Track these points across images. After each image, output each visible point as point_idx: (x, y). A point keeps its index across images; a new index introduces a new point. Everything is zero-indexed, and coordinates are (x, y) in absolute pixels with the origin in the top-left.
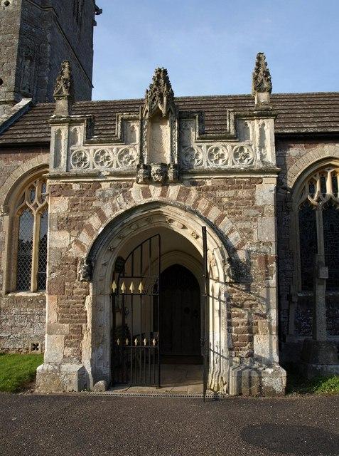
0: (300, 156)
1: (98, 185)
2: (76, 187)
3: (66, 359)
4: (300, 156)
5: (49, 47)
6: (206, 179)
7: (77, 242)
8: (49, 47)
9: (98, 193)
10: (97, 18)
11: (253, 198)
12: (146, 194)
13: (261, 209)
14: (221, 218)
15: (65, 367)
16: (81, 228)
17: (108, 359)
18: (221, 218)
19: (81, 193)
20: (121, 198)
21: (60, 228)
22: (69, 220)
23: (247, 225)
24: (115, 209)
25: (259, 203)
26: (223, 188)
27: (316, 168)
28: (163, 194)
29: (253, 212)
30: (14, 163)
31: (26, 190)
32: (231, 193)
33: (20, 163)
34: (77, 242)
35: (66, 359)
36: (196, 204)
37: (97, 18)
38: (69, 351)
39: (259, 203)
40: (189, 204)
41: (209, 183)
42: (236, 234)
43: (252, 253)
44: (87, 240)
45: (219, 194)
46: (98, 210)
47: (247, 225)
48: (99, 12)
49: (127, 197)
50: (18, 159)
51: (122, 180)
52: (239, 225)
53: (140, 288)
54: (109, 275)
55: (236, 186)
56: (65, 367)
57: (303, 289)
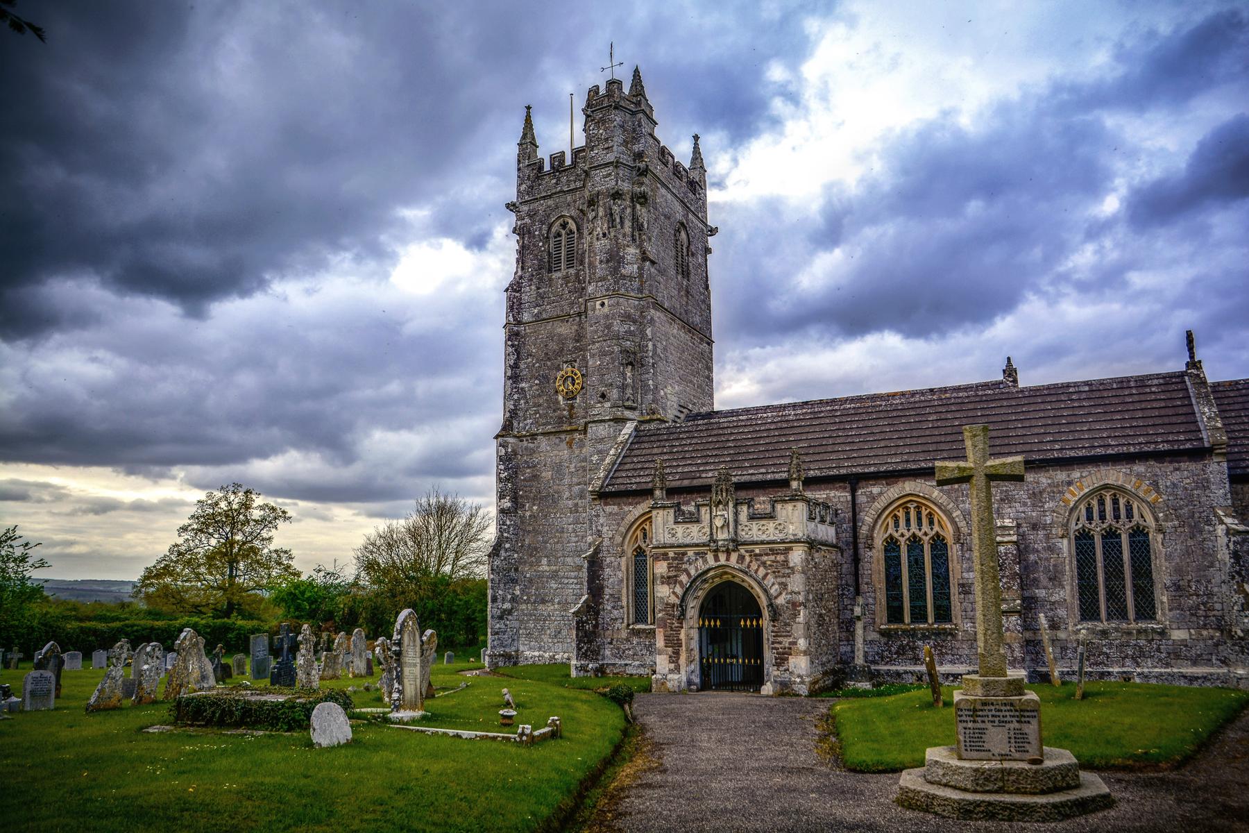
0: (881, 494)
1: (684, 554)
2: (671, 555)
3: (671, 671)
4: (881, 494)
5: (650, 345)
7: (674, 593)
10: (711, 241)
11: (786, 561)
12: (717, 559)
13: (792, 568)
15: (669, 676)
17: (698, 672)
21: (663, 583)
23: (784, 580)
25: (791, 565)
26: (767, 554)
27: (887, 512)
28: (728, 560)
29: (787, 571)
30: (626, 509)
32: (772, 558)
34: (674, 593)
35: (671, 671)
36: (749, 567)
37: (711, 241)
39: (791, 565)
40: (743, 567)
41: (757, 551)
47: (784, 580)
49: (705, 561)
50: (630, 504)
52: (779, 580)
53: (718, 623)
54: (696, 616)
55: (773, 552)
56: (669, 676)
57: (889, 621)
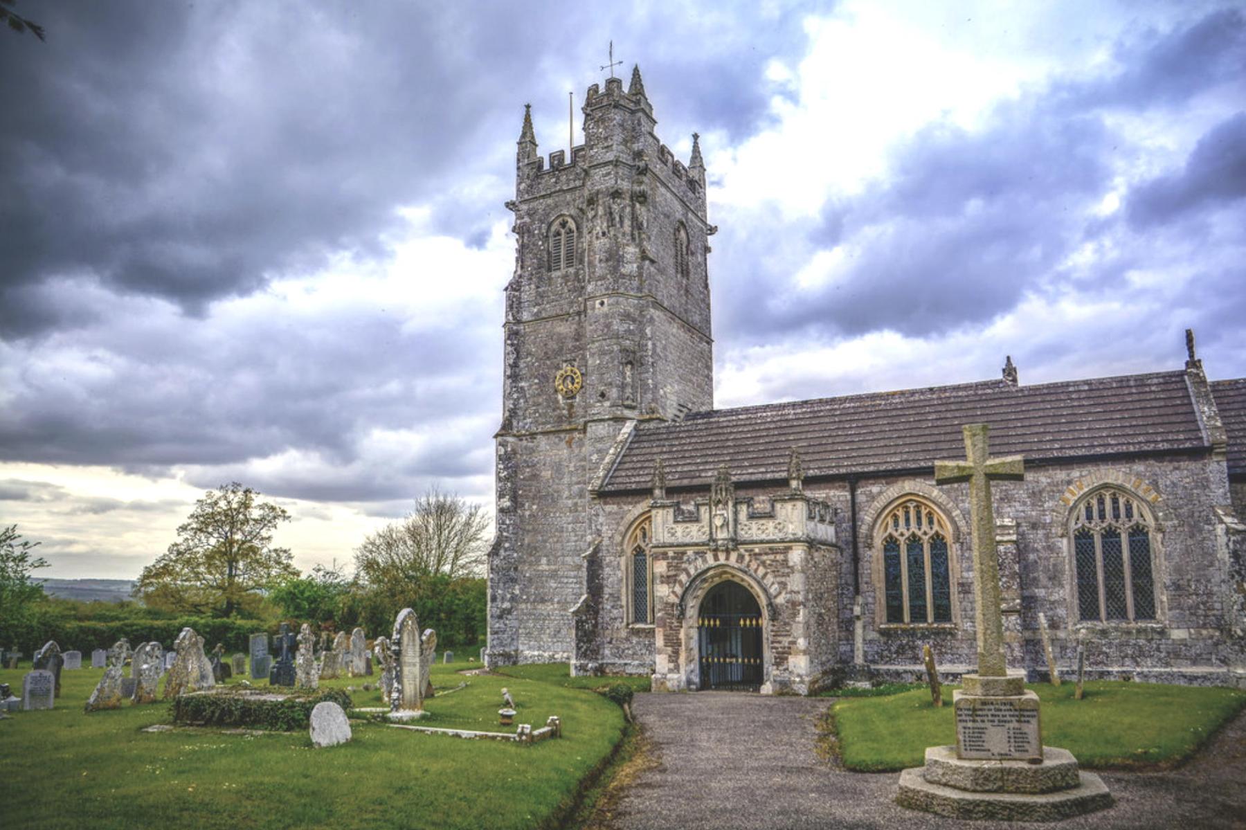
0: (880, 493)
2: (671, 554)
3: (671, 671)
4: (880, 493)
5: (650, 343)
6: (575, 698)
8: (650, 343)
9: (685, 558)
12: (716, 558)
14: (766, 574)
15: (669, 676)
16: (675, 582)
17: (697, 671)
18: (766, 574)
19: (673, 558)
20: (699, 561)
21: (662, 582)
22: (668, 577)
23: (783, 579)
24: (696, 569)
25: (791, 564)
26: (766, 554)
29: (787, 570)
30: (626, 508)
31: (638, 531)
32: (772, 557)
33: (630, 507)
34: (674, 592)
35: (671, 671)
38: (672, 665)
39: (791, 564)
40: (743, 566)
41: (757, 550)
42: (776, 586)
43: (285, 727)
44: (678, 590)
45: (765, 557)
46: (686, 570)
47: (783, 579)
48: (713, 230)
49: (705, 561)
50: (630, 503)
51: (701, 548)
52: (778, 579)
53: (742, 622)
55: (773, 551)
56: (669, 676)
